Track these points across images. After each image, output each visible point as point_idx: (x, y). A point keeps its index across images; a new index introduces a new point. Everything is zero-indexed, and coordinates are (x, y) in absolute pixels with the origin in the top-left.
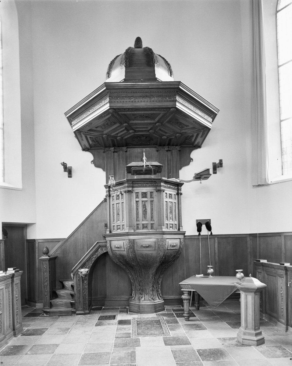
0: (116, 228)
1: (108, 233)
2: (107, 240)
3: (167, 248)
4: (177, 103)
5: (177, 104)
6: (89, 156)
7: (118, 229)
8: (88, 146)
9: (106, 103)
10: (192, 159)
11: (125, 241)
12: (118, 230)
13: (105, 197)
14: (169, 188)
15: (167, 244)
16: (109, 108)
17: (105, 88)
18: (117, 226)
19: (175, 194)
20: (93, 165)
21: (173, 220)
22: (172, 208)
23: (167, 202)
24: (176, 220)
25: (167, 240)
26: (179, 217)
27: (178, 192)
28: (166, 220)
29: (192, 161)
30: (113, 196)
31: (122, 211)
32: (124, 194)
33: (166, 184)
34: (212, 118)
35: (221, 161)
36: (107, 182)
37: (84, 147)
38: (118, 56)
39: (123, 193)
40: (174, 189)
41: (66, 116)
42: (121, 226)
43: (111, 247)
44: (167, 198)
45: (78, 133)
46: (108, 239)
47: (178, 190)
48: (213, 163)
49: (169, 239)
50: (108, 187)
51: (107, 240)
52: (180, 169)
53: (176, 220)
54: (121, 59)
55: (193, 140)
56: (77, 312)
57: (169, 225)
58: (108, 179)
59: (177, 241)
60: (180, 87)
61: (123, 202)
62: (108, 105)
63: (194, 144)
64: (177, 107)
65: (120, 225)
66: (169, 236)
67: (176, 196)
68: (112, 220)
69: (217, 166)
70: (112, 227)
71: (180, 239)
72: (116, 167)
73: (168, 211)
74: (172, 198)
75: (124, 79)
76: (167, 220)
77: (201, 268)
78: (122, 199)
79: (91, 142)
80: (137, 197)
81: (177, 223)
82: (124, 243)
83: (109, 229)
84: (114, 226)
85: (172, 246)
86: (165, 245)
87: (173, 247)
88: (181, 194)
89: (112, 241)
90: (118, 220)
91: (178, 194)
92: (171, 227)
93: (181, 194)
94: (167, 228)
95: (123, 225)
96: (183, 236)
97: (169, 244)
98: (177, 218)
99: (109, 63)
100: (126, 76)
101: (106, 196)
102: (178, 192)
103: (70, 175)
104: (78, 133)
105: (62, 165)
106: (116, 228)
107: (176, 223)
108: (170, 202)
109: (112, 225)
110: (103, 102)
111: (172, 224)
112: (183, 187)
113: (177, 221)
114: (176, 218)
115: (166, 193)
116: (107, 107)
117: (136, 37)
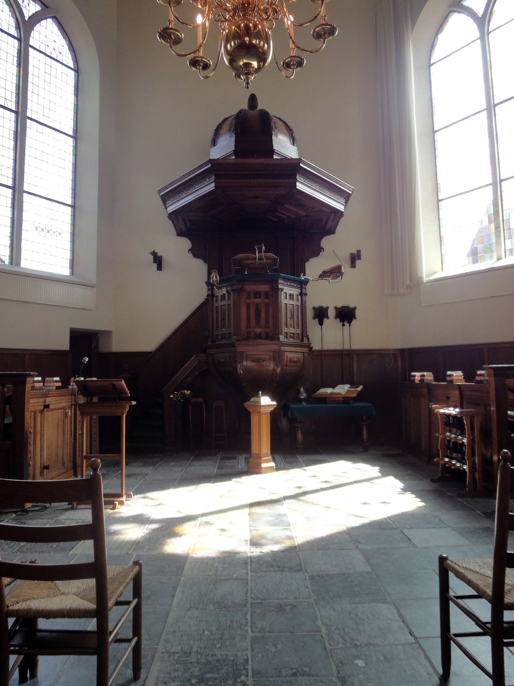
1: (210, 343)
4: (297, 183)
5: (298, 184)
6: (186, 243)
7: (222, 339)
9: (211, 183)
10: (323, 249)
15: (286, 359)
16: (214, 188)
17: (210, 165)
19: (298, 294)
20: (191, 254)
21: (294, 328)
25: (286, 353)
33: (285, 281)
34: (345, 198)
35: (359, 251)
36: (209, 278)
38: (226, 119)
39: (230, 291)
41: (159, 194)
44: (286, 299)
45: (173, 216)
47: (301, 288)
52: (307, 261)
54: (230, 124)
57: (288, 334)
58: (209, 274)
59: (300, 356)
60: (301, 165)
62: (213, 185)
64: (297, 187)
66: (289, 348)
67: (299, 297)
68: (215, 326)
69: (355, 258)
71: (303, 353)
74: (293, 300)
75: (234, 150)
76: (287, 327)
80: (249, 297)
81: (299, 331)
84: (217, 335)
88: (306, 294)
90: (223, 326)
91: (301, 294)
93: (154, 262)
96: (308, 349)
98: (300, 325)
99: (215, 127)
100: (235, 146)
103: (159, 268)
104: (173, 216)
105: (152, 254)
109: (216, 333)
110: (207, 180)
111: (294, 334)
112: (308, 287)
113: (300, 328)
115: (286, 293)
116: (211, 187)
117: (250, 94)
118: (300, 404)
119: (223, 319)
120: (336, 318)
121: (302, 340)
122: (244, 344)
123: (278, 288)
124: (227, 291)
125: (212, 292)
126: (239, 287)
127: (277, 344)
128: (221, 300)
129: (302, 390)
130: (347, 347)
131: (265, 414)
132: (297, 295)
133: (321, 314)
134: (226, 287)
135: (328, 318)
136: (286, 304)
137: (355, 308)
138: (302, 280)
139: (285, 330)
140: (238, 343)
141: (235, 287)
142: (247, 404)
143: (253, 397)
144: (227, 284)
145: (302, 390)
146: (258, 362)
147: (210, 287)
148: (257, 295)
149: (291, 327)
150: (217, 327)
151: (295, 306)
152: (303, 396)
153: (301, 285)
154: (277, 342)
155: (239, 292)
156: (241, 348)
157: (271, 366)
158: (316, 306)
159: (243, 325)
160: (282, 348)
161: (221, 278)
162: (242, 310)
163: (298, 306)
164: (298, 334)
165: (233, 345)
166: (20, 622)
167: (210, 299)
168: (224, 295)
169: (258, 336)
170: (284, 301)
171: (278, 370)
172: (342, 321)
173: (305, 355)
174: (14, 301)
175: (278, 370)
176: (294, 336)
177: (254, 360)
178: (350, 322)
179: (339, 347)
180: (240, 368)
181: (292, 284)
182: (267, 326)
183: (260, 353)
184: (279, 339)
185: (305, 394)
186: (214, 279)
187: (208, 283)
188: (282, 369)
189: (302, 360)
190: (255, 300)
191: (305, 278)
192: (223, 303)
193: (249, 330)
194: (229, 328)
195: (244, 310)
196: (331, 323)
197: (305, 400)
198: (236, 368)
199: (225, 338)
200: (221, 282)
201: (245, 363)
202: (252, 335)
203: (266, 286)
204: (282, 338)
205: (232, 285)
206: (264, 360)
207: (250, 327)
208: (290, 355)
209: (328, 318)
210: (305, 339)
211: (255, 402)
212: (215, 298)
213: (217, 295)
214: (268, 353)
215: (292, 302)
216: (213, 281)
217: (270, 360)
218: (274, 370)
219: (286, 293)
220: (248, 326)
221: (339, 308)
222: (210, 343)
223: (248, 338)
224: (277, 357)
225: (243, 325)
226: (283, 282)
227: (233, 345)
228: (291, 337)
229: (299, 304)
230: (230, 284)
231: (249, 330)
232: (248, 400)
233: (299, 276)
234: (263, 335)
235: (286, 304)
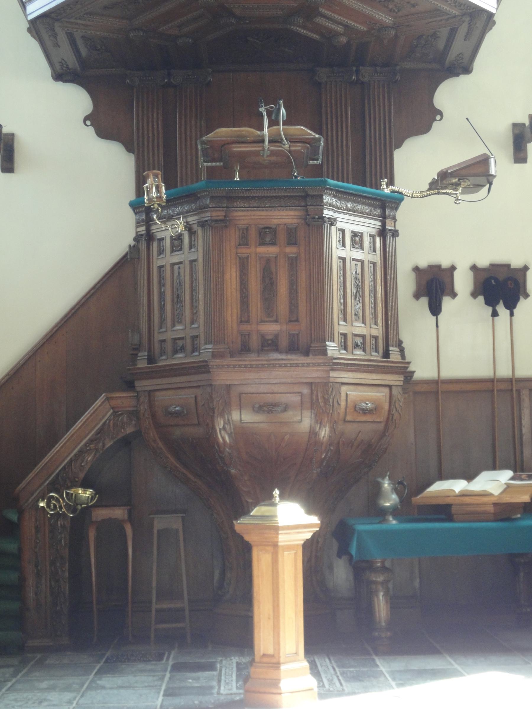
0: (169, 347)
1: (142, 364)
2: (138, 389)
3: (342, 415)
6: (76, 100)
7: (175, 352)
8: (72, 61)
10: (440, 113)
11: (199, 392)
12: (176, 356)
13: (133, 243)
14: (353, 211)
15: (343, 404)
18: (175, 339)
19: (374, 232)
20: (91, 130)
21: (364, 322)
22: (363, 282)
23: (344, 260)
24: (376, 323)
25: (344, 389)
26: (386, 314)
27: (384, 225)
28: (342, 323)
29: (438, 117)
30: (163, 239)
31: (193, 290)
32: (200, 232)
33: (340, 199)
36: (139, 192)
37: (62, 69)
39: (195, 227)
40: (369, 216)
42: (188, 341)
43: (153, 415)
44: (344, 245)
46: (142, 385)
47: (383, 218)
48: (515, 125)
49: (351, 387)
50: (141, 209)
51: (138, 389)
52: (399, 145)
53: (376, 323)
55: (441, 44)
56: (31, 643)
57: (349, 337)
59: (382, 395)
61: (195, 261)
63: (447, 62)
65: (182, 338)
67: (378, 239)
70: (157, 346)
71: (390, 387)
72: (244, 133)
73: (348, 291)
76: (345, 320)
77: (176, 118)
78: (193, 250)
79: (84, 52)
81: (378, 331)
82: (199, 399)
83: (146, 354)
85: (363, 410)
86: (336, 404)
87: (365, 413)
89: (157, 393)
90: (177, 319)
91: (382, 233)
92: (357, 345)
94: (345, 348)
95: (194, 338)
97: (350, 404)
101: (137, 239)
102: (384, 225)
106: (169, 347)
107: (375, 332)
108: (354, 260)
109: (158, 337)
111: (363, 337)
114: (376, 317)
120: (474, 295)
130: (504, 371)
133: (434, 286)
135: (454, 295)
137: (526, 268)
158: (423, 264)
165: (203, 368)
172: (491, 302)
178: (511, 306)
179: (483, 371)
189: (386, 406)
196: (463, 308)
208: (354, 394)
209: (454, 295)
221: (484, 270)
222: (142, 364)
228: (356, 346)
233: (378, 186)
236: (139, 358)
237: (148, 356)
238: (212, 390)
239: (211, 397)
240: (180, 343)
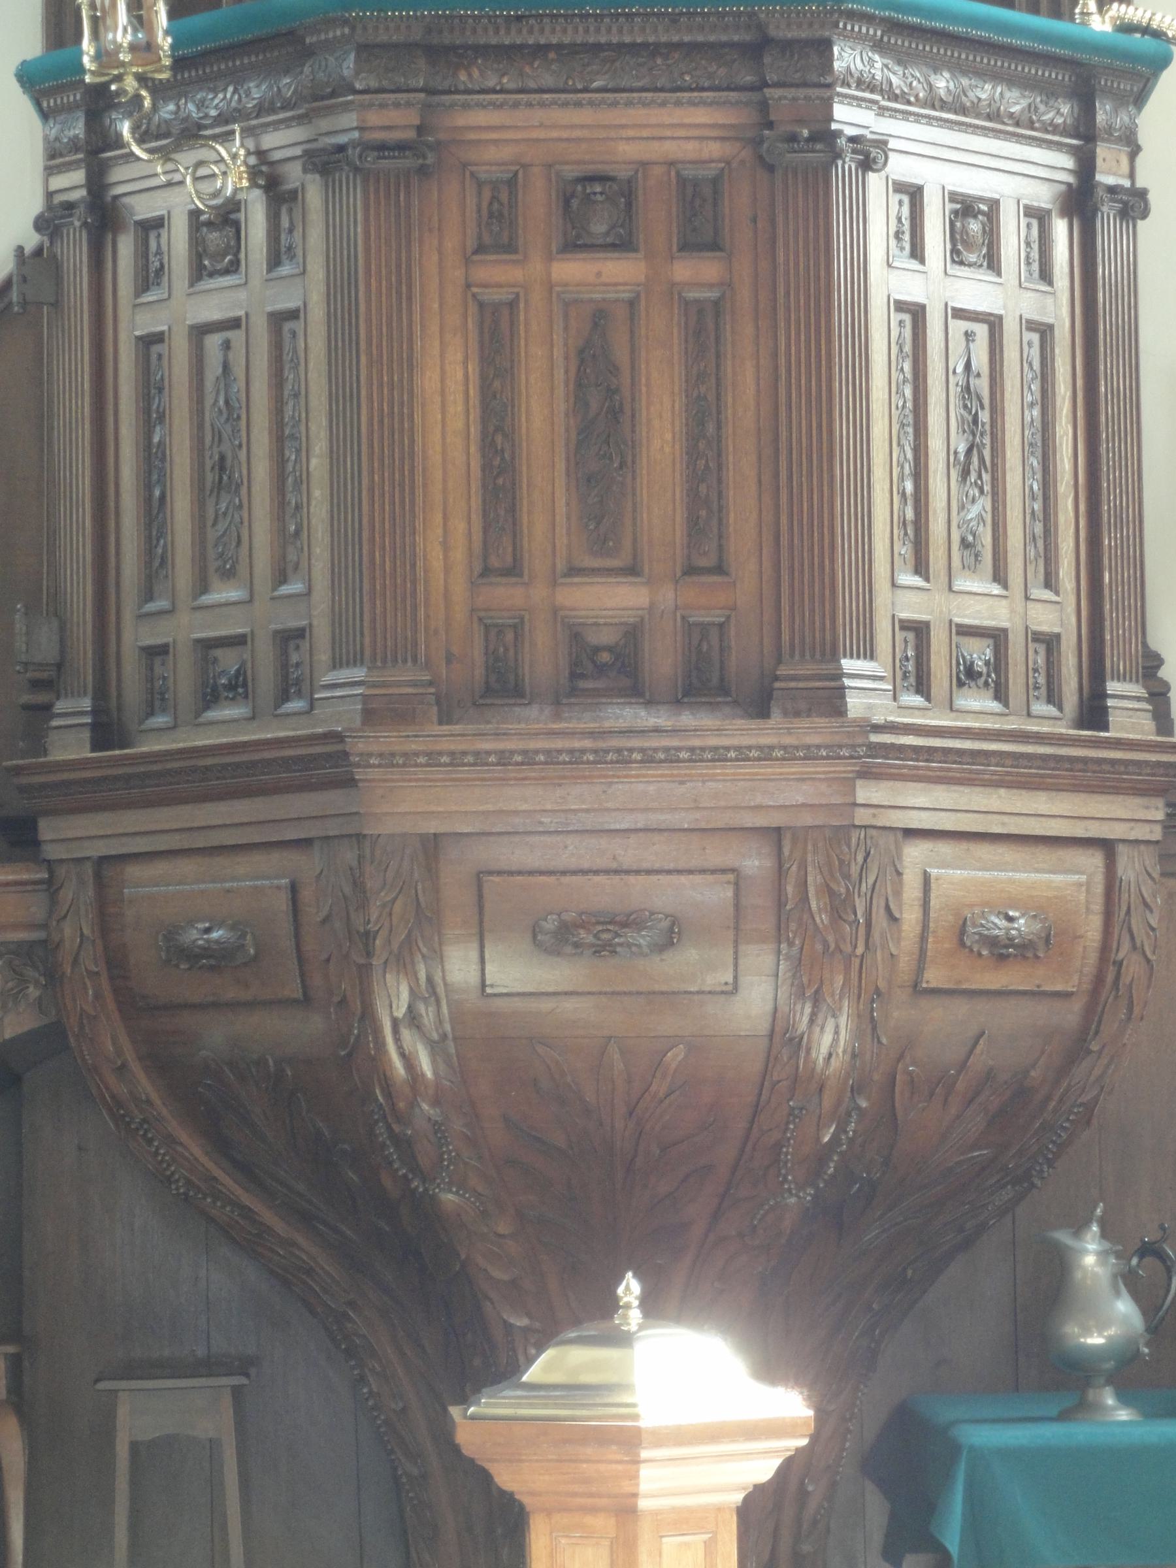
1: (70, 746)
7: (210, 696)
12: (211, 715)
15: (910, 917)
18: (207, 645)
19: (1043, 196)
21: (999, 576)
25: (915, 854)
33: (903, 59)
39: (294, 174)
44: (917, 252)
47: (1084, 138)
51: (52, 852)
57: (939, 640)
59: (1071, 880)
65: (239, 641)
66: (942, 796)
67: (1060, 228)
71: (1107, 847)
76: (921, 567)
81: (1057, 613)
83: (86, 704)
89: (134, 871)
90: (218, 560)
91: (1080, 200)
109: (134, 635)
111: (998, 637)
115: (915, 194)
118: (1064, 1416)
119: (220, 477)
121: (1093, 712)
122: (456, 760)
123: (826, 137)
124: (267, 176)
125: (97, 184)
126: (395, 119)
127: (810, 754)
128: (198, 272)
129: (1091, 1257)
131: (683, 1521)
132: (1039, 216)
134: (251, 119)
136: (917, 313)
138: (1097, 47)
139: (900, 596)
140: (388, 739)
141: (344, 126)
142: (483, 1422)
143: (545, 1337)
144: (257, 91)
145: (1091, 1257)
146: (603, 949)
147: (78, 129)
148: (597, 205)
149: (972, 565)
150: (156, 565)
151: (1011, 328)
152: (1106, 1321)
153: (1085, 99)
154: (814, 731)
155: (395, 171)
156: (407, 802)
157: (750, 993)
159: (445, 543)
160: (867, 792)
161: (198, 21)
162: (428, 381)
163: (1045, 331)
164: (1050, 642)
165: (324, 766)
166: (239, 1191)
167: (75, 252)
168: (228, 216)
169: (606, 668)
170: (892, 276)
171: (831, 1040)
173: (1129, 867)
174: (264, 822)
175: (831, 1040)
176: (999, 663)
177: (566, 935)
180: (413, 1017)
181: (985, 92)
182: (703, 558)
183: (629, 853)
184: (831, 700)
185: (1124, 1307)
186: (121, 33)
187: (47, 85)
188: (868, 1025)
190: (573, 270)
191: (1127, 28)
192: (214, 303)
193: (505, 596)
194: (281, 578)
195: (446, 381)
197: (1128, 1372)
198: (368, 1015)
199: (239, 687)
200: (195, 64)
201: (459, 966)
202: (542, 656)
203: (701, 116)
204: (869, 688)
205: (320, 99)
206: (672, 935)
207: (513, 570)
208: (958, 876)
210: (1122, 692)
211: (573, 1390)
212: (126, 246)
213: (143, 208)
214: (715, 857)
215: (975, 291)
216: (104, 56)
217: (737, 926)
218: (1086, 1251)
219: (915, 194)
220: (500, 560)
222: (70, 746)
223: (502, 686)
224: (816, 888)
225: (445, 543)
226: (878, 66)
227: (324, 766)
228: (968, 675)
229: (1057, 306)
230: (287, 85)
231: (505, 596)
232: (501, 1368)
234: (663, 659)
235: (917, 313)
236: (55, 723)
237: (95, 712)
238: (360, 858)
239: (358, 884)
240: (229, 661)
